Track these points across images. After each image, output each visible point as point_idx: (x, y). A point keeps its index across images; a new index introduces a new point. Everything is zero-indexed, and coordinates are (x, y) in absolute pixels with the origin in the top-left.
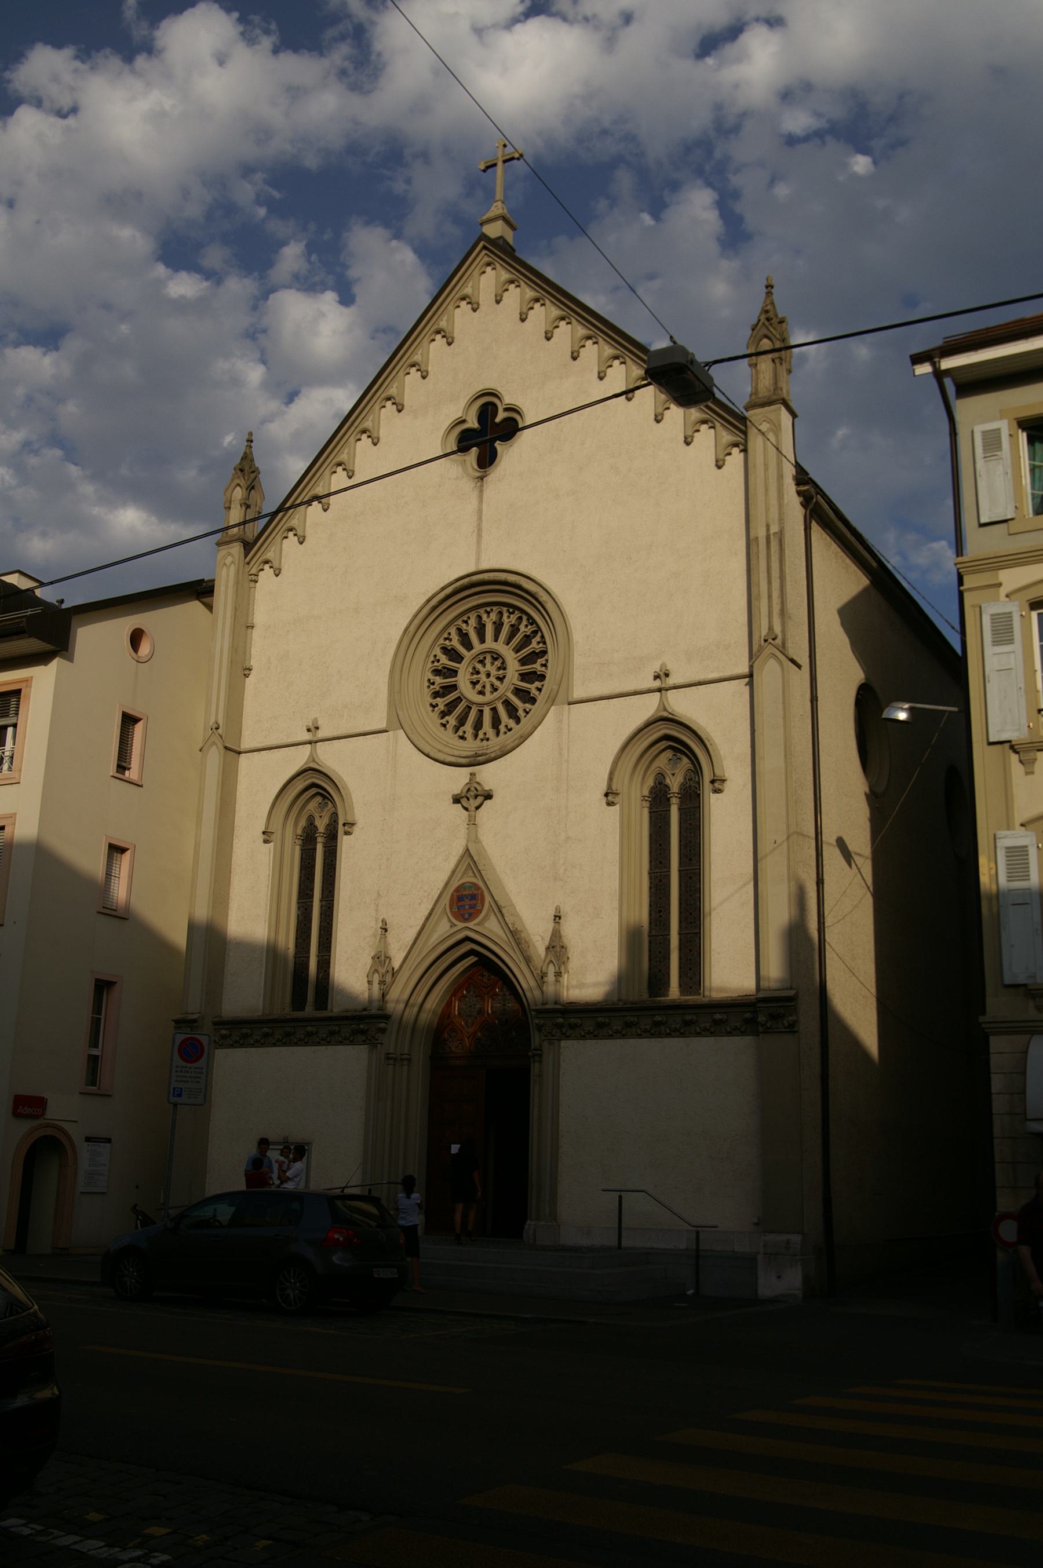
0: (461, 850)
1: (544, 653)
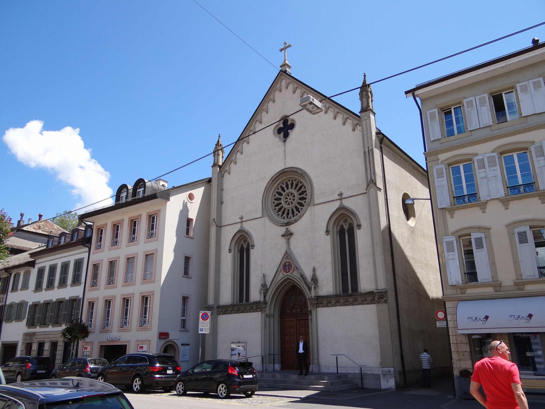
0: (285, 252)
1: (306, 191)
